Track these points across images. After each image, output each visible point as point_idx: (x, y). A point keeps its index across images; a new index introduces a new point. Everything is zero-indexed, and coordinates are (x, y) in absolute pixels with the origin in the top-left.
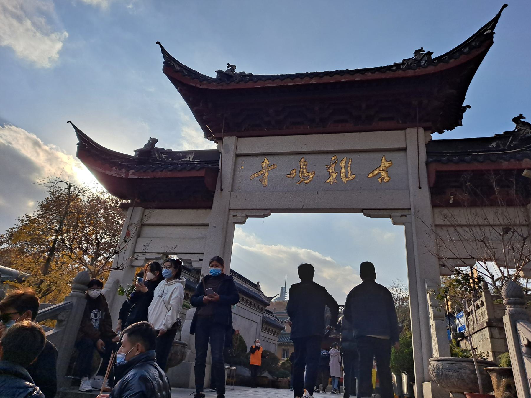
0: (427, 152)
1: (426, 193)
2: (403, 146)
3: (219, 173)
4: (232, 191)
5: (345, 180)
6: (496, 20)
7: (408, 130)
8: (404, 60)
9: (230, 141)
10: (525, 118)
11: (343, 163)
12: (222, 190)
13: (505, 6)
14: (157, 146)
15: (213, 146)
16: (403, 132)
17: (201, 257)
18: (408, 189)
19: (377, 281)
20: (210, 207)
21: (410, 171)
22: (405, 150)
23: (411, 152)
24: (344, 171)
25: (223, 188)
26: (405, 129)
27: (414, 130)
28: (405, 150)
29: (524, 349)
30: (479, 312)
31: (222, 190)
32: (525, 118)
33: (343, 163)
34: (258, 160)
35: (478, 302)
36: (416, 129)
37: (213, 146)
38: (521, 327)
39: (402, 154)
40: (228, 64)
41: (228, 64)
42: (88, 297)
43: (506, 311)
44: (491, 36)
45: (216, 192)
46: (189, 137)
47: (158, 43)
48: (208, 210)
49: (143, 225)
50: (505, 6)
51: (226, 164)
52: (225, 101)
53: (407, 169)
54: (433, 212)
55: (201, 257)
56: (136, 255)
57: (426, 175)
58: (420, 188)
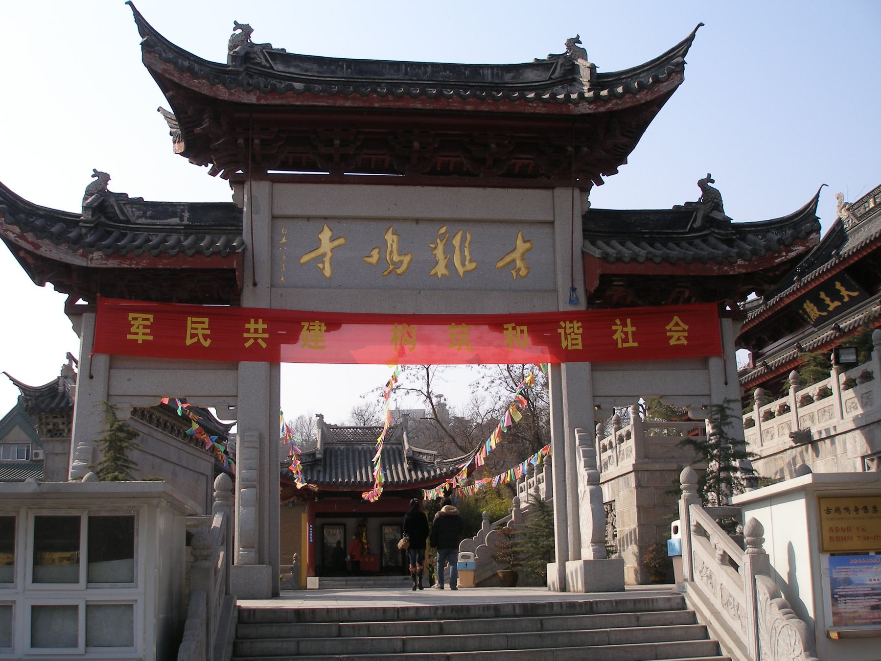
0: (584, 230)
2: (550, 218)
4: (272, 286)
5: (461, 271)
6: (687, 43)
7: (558, 191)
8: (552, 56)
10: (713, 181)
11: (456, 242)
12: (255, 284)
13: (701, 25)
15: (209, 187)
18: (556, 291)
21: (559, 261)
22: (552, 223)
25: (257, 280)
27: (569, 191)
29: (692, 528)
31: (255, 284)
32: (713, 181)
34: (320, 233)
36: (570, 191)
37: (209, 187)
38: (692, 508)
39: (547, 229)
40: (235, 23)
41: (235, 23)
43: (682, 496)
44: (680, 68)
50: (701, 25)
51: (255, 232)
52: (232, 104)
53: (555, 256)
57: (581, 271)
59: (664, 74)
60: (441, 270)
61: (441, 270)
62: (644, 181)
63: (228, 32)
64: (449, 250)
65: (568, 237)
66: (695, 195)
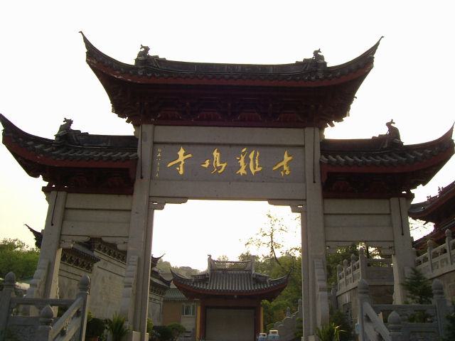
1: (318, 186)
3: (139, 161)
9: (148, 128)
11: (251, 156)
12: (142, 178)
14: (73, 127)
15: (124, 128)
16: (302, 130)
17: (125, 240)
19: (156, 212)
20: (132, 194)
22: (303, 146)
23: (309, 147)
24: (249, 163)
26: (304, 127)
28: (303, 146)
30: (355, 272)
33: (251, 156)
35: (355, 264)
37: (124, 128)
42: (171, 281)
45: (137, 180)
46: (101, 118)
47: (81, 32)
48: (130, 196)
49: (66, 209)
51: (144, 150)
52: (146, 88)
54: (323, 203)
55: (125, 240)
56: (63, 238)
58: (314, 182)
59: (363, 65)
60: (242, 171)
61: (242, 171)
62: (358, 124)
63: (138, 50)
64: (247, 161)
65: (313, 156)
66: (384, 131)
